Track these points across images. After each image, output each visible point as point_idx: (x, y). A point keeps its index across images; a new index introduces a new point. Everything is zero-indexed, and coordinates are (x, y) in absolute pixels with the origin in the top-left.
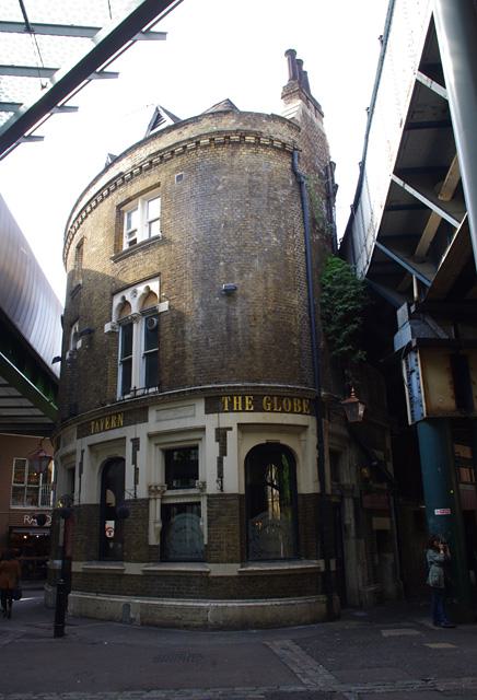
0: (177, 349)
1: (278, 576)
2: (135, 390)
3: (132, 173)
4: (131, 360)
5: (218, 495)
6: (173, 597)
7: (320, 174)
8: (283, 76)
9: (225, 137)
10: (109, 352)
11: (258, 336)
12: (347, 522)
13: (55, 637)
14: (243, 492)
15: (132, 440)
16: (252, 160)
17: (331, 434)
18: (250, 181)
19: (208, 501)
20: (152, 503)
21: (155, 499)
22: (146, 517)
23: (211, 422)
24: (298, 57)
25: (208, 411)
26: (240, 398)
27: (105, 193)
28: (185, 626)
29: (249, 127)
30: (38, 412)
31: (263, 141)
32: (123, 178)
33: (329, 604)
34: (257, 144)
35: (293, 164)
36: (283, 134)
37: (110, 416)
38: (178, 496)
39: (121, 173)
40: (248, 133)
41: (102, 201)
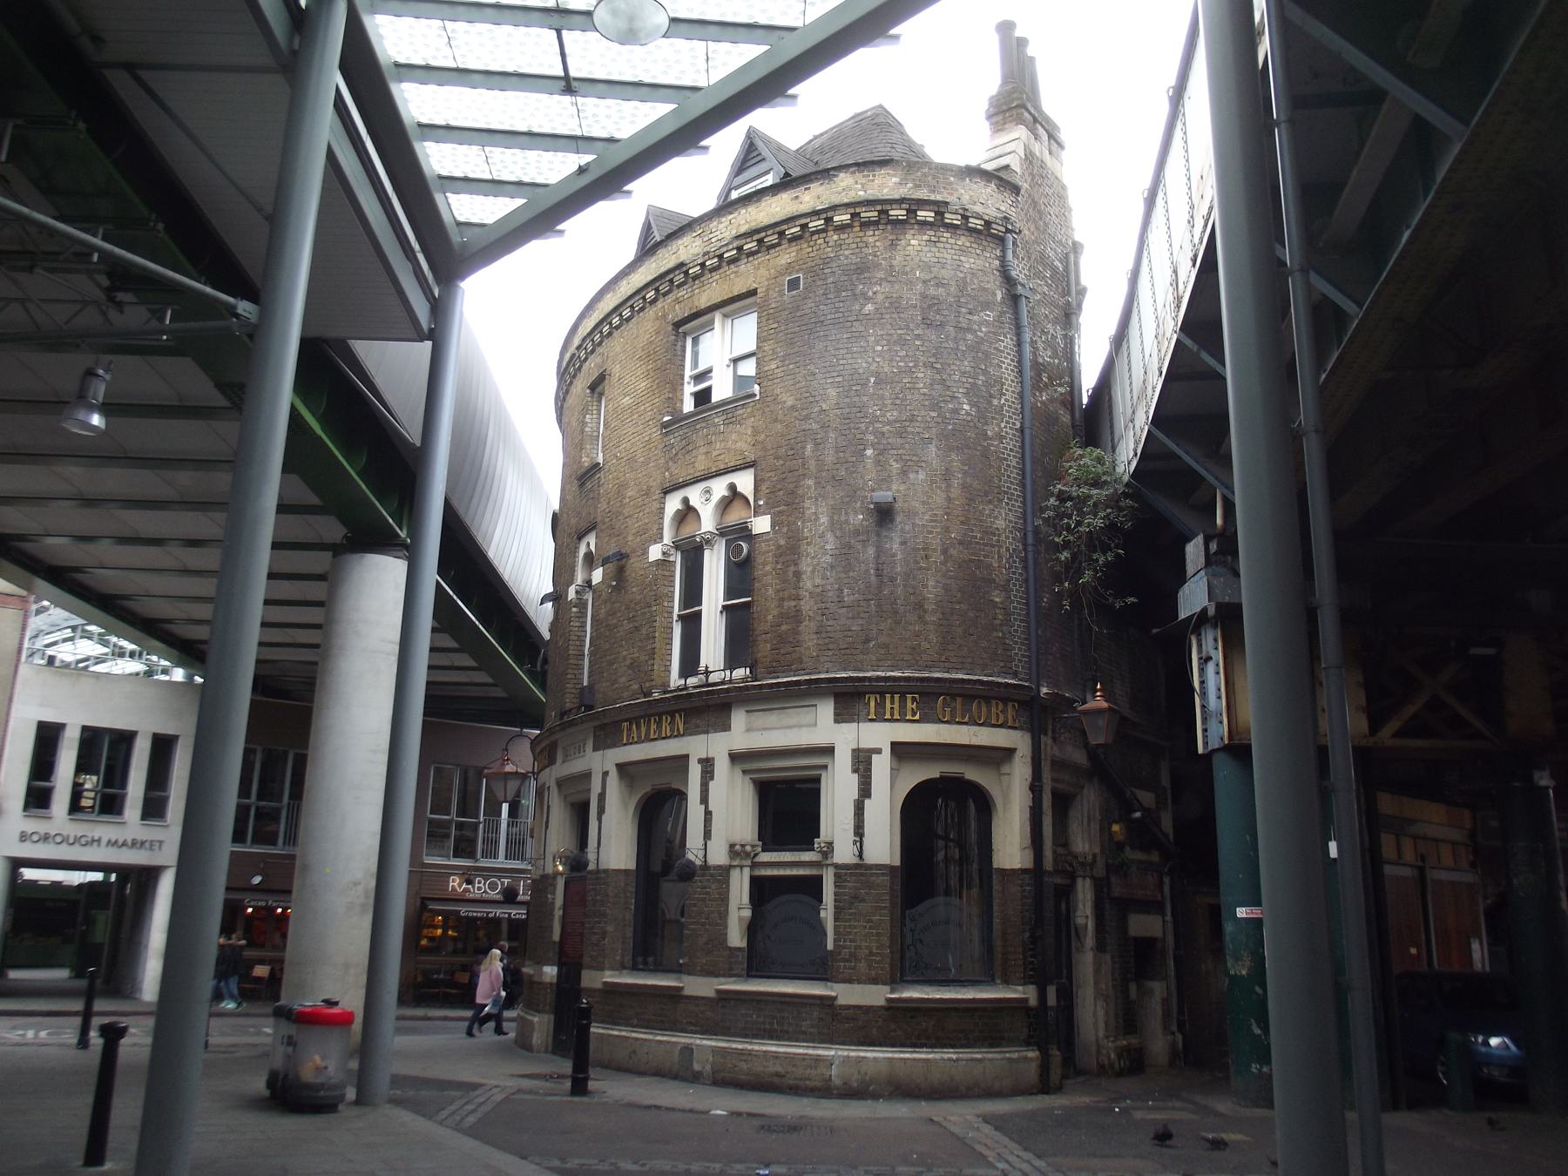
0: (786, 604)
1: (956, 1009)
2: (707, 672)
3: (703, 265)
4: (698, 615)
5: (856, 866)
6: (771, 1038)
7: (1054, 270)
8: (990, 81)
9: (880, 212)
10: (658, 598)
11: (932, 589)
12: (1080, 921)
13: (1045, 1087)
14: (897, 862)
15: (700, 761)
16: (929, 255)
17: (1057, 764)
18: (924, 296)
19: (836, 875)
20: (735, 874)
21: (741, 867)
22: (724, 899)
23: (846, 737)
24: (1018, 33)
25: (839, 718)
26: (897, 697)
27: (651, 294)
28: (791, 1088)
29: (923, 194)
30: (482, 677)
31: (950, 218)
32: (686, 273)
33: (1044, 1068)
34: (939, 223)
35: (1003, 259)
36: (987, 202)
37: (660, 715)
38: (785, 862)
39: (682, 265)
40: (923, 203)
41: (642, 309)
